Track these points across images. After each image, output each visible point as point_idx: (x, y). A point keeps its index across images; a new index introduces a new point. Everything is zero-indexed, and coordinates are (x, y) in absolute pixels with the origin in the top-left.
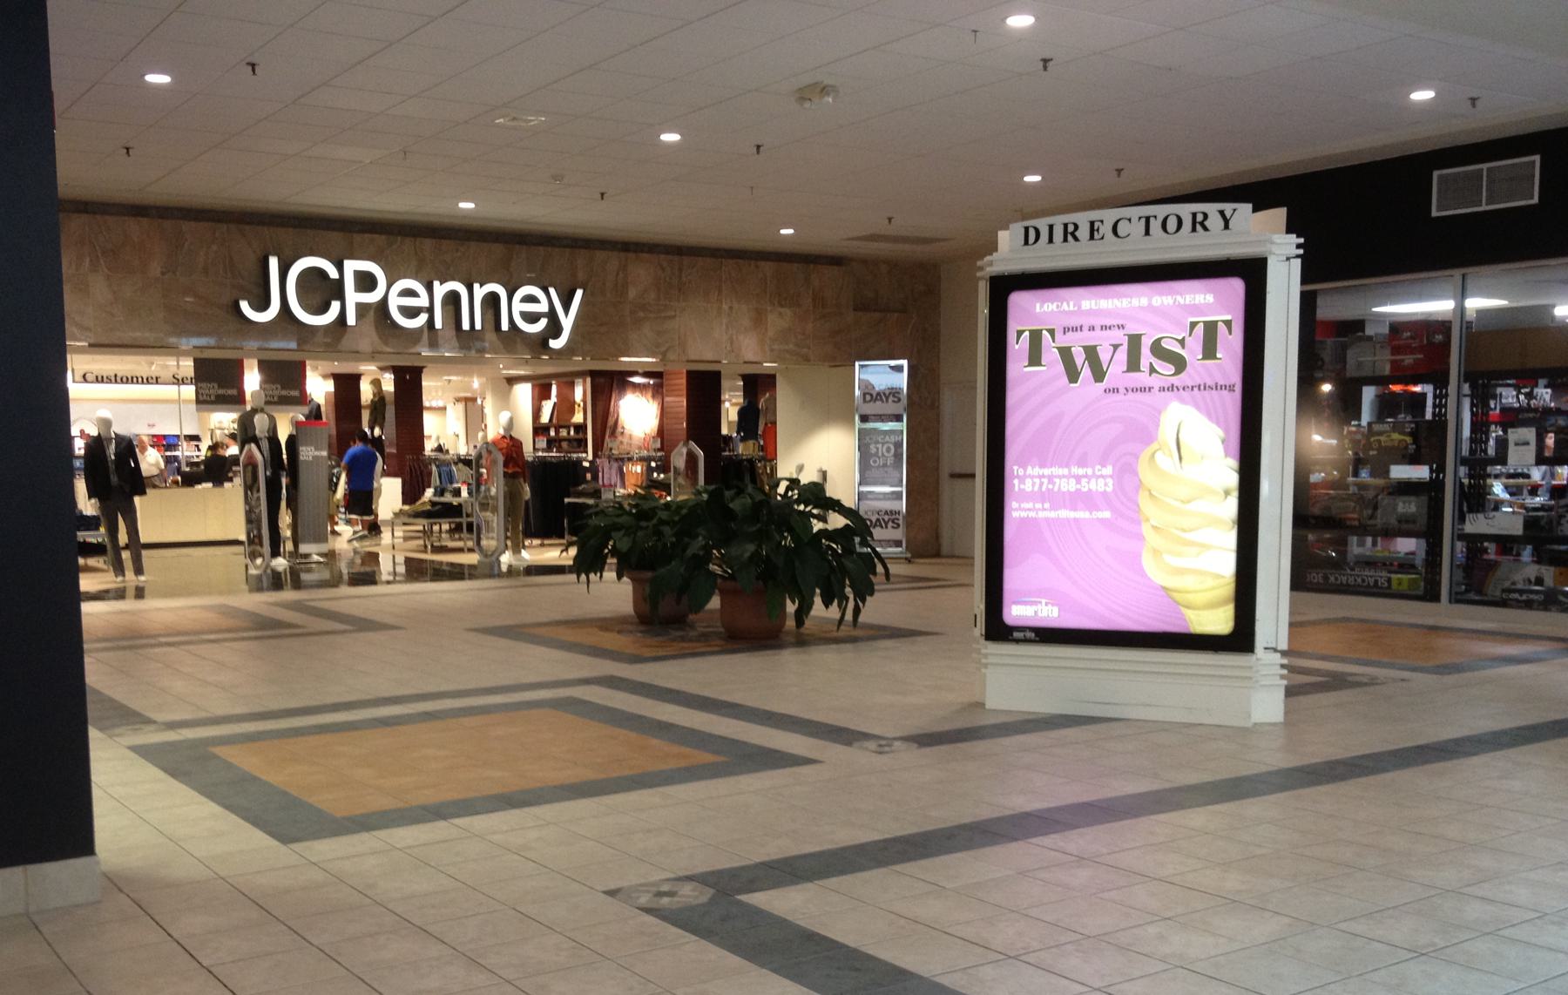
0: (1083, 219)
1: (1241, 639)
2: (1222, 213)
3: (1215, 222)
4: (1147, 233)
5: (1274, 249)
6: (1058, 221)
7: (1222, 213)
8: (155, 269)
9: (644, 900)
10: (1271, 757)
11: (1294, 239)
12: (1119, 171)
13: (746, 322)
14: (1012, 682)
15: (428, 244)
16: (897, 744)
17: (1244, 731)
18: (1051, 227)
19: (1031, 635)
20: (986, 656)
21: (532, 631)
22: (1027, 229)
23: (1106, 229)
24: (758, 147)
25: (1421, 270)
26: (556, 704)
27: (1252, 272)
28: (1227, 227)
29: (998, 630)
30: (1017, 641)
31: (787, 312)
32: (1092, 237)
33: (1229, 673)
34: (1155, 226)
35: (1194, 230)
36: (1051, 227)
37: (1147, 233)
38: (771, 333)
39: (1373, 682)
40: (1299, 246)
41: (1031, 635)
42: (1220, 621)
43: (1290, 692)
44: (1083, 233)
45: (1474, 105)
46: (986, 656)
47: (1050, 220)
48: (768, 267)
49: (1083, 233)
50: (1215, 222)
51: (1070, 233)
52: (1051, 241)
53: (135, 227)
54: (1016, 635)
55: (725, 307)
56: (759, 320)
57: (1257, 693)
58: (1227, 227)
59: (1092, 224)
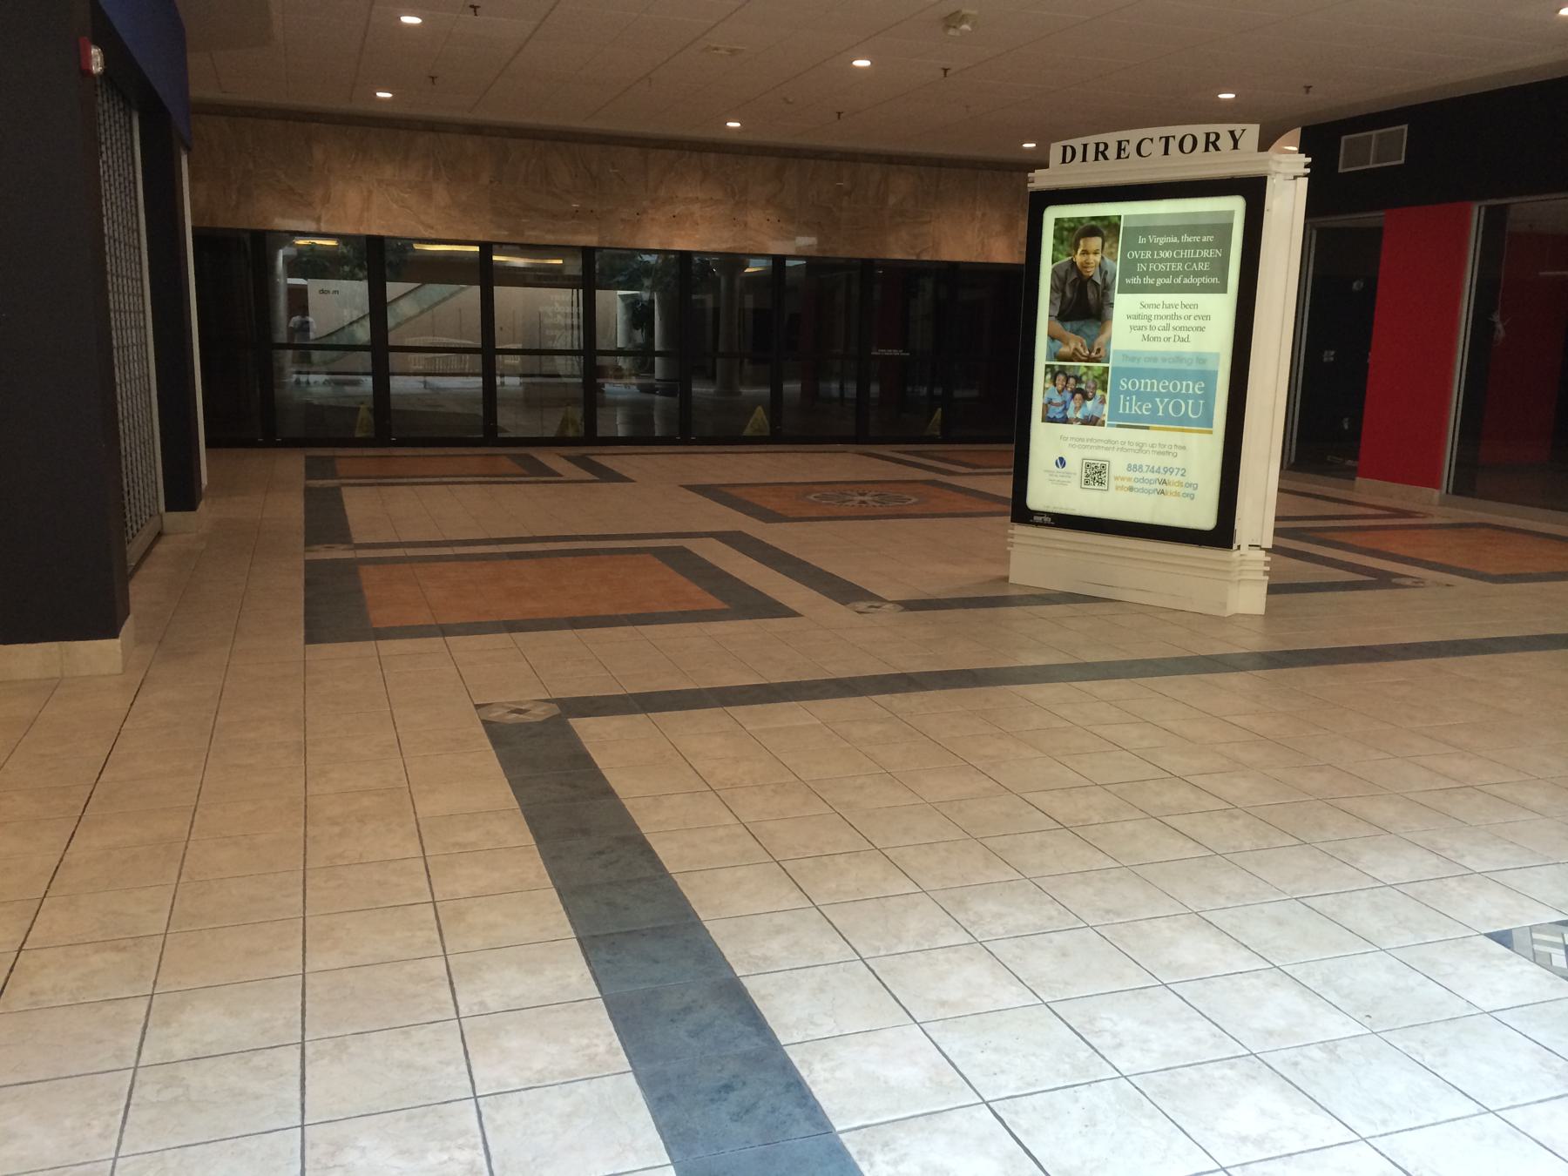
0: (1111, 138)
1: (1222, 535)
2: (1232, 133)
3: (1225, 142)
4: (1166, 153)
5: (1274, 167)
6: (1091, 140)
7: (1232, 133)
9: (495, 715)
10: (1252, 642)
12: (1308, 88)
14: (1033, 559)
15: (712, 157)
17: (1220, 621)
18: (1085, 146)
19: (1047, 519)
20: (1012, 536)
21: (734, 492)
22: (1065, 148)
23: (1131, 149)
24: (946, 70)
25: (1529, 194)
26: (659, 553)
27: (1253, 190)
28: (1235, 147)
29: (1022, 514)
30: (1037, 524)
32: (1119, 157)
33: (1176, 561)
34: (1173, 145)
35: (1207, 150)
36: (1085, 146)
37: (1166, 153)
41: (1047, 519)
42: (1205, 519)
43: (1272, 589)
44: (1112, 152)
46: (1012, 536)
47: (1084, 140)
49: (1112, 152)
50: (1225, 142)
51: (1101, 153)
52: (1084, 160)
54: (1037, 519)
55: (979, 213)
57: (1241, 586)
58: (1235, 147)
59: (1120, 143)
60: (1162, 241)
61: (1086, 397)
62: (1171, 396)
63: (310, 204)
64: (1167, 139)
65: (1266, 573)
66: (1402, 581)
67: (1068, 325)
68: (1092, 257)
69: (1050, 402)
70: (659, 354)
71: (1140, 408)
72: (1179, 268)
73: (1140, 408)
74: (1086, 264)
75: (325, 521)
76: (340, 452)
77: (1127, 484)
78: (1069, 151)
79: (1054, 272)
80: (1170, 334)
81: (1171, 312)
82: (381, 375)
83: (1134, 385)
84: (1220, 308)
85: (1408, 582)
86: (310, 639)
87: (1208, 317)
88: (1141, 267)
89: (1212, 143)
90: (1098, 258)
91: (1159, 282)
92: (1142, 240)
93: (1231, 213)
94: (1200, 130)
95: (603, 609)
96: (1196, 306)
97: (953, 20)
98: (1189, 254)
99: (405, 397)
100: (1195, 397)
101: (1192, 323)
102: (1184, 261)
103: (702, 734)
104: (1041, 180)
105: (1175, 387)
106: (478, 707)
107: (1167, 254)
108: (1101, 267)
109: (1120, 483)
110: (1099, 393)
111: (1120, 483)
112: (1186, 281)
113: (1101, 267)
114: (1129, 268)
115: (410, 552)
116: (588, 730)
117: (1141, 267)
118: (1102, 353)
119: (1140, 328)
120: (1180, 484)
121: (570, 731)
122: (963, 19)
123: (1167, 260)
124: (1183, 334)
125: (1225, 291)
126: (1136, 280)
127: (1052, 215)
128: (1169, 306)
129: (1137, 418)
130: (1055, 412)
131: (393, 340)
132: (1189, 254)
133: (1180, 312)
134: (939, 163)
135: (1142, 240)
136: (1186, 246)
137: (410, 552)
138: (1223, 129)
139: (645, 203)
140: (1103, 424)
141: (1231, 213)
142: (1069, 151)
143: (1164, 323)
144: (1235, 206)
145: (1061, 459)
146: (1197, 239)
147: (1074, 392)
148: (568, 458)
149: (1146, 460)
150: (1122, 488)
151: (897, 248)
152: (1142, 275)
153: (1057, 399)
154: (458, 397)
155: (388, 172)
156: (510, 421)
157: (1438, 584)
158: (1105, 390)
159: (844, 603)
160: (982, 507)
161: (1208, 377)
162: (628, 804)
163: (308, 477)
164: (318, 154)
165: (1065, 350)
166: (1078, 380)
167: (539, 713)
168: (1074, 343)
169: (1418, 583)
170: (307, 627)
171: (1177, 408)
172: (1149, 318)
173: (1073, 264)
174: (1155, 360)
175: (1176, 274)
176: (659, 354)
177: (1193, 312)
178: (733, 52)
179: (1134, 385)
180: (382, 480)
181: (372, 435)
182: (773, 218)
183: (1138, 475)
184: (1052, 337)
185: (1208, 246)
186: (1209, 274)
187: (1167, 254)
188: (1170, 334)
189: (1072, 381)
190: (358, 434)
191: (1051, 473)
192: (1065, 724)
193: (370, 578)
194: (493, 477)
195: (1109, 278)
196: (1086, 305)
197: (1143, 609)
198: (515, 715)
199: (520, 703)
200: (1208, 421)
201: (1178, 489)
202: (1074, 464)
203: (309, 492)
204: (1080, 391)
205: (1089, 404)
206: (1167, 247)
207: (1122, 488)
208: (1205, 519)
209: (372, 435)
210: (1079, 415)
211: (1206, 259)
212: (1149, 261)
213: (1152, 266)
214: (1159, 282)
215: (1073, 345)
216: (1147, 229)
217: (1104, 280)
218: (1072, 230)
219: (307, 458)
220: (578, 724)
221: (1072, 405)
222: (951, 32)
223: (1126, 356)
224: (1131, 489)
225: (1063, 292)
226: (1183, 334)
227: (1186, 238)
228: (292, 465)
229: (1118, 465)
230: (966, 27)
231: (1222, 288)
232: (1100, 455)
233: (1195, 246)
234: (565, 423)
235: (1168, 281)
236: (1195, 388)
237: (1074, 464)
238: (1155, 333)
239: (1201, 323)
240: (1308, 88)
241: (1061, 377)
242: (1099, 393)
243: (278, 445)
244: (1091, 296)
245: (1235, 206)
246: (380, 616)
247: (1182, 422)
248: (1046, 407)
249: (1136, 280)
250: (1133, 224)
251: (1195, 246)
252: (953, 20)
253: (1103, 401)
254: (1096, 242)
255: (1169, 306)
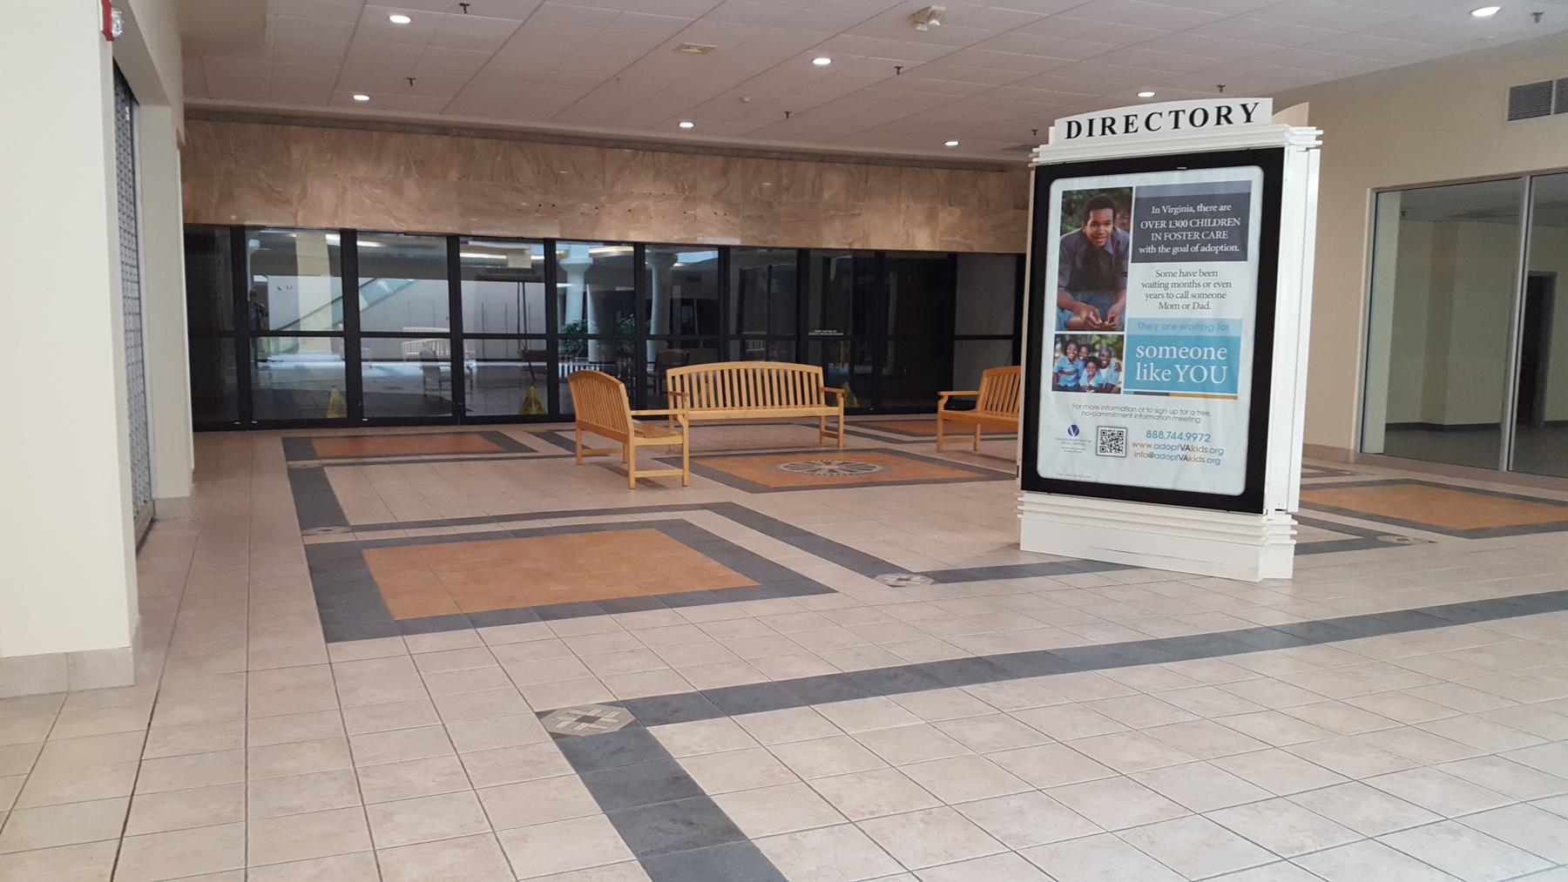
1: (1251, 500)
2: (1244, 106)
3: (1238, 115)
4: (1176, 126)
5: (1292, 140)
6: (1097, 116)
7: (1244, 106)
8: (453, 175)
9: (562, 725)
11: (1314, 132)
13: (920, 218)
14: (1046, 526)
16: (917, 578)
18: (1091, 121)
20: (1022, 503)
23: (1139, 123)
26: (663, 526)
27: (1271, 161)
28: (1248, 120)
31: (957, 211)
32: (1127, 131)
36: (1091, 121)
37: (1176, 126)
38: (941, 228)
39: (1403, 542)
40: (1318, 138)
42: (1234, 485)
43: (1301, 549)
44: (1119, 126)
45: (1537, 20)
46: (1022, 503)
47: (1090, 115)
48: (941, 174)
49: (1119, 126)
50: (1238, 115)
53: (439, 143)
56: (931, 217)
57: (1268, 546)
58: (1248, 120)
60: (1176, 211)
61: (1099, 365)
62: (1193, 362)
63: (288, 202)
64: (1177, 113)
65: (1292, 537)
66: (1387, 539)
67: (1079, 295)
68: (1103, 228)
69: (1061, 371)
70: (592, 337)
71: (1159, 375)
72: (1196, 236)
73: (1159, 375)
74: (1097, 235)
75: (317, 507)
76: (314, 433)
77: (1147, 451)
78: (1074, 126)
79: (1063, 243)
80: (1189, 301)
81: (1189, 279)
82: (353, 360)
83: (1151, 352)
84: (1242, 276)
85: (1394, 540)
86: (330, 637)
87: (1228, 285)
88: (1156, 237)
89: (1224, 116)
90: (1110, 229)
91: (1176, 250)
92: (1156, 211)
93: (1249, 183)
94: (1211, 105)
95: (631, 591)
96: (1215, 273)
97: (923, 15)
98: (1206, 222)
99: (375, 380)
100: (1219, 363)
101: (1212, 290)
102: (1200, 229)
103: (793, 733)
104: (1047, 154)
105: (1196, 354)
106: (540, 715)
107: (1183, 224)
108: (1113, 236)
109: (1138, 450)
110: (1114, 361)
111: (1138, 450)
112: (1204, 249)
113: (1113, 236)
114: (1143, 238)
115: (412, 533)
116: (675, 738)
117: (1156, 237)
118: (1116, 321)
119: (1157, 297)
120: (1205, 450)
121: (653, 746)
122: (933, 15)
123: (1183, 229)
124: (1203, 302)
125: (1245, 259)
126: (1151, 249)
127: (1058, 188)
128: (1187, 274)
129: (1155, 384)
130: (1067, 380)
131: (365, 326)
132: (1206, 222)
133: (1197, 279)
134: (868, 161)
135: (1156, 211)
136: (1201, 215)
137: (412, 533)
138: (1235, 103)
139: (603, 198)
140: (1119, 391)
141: (1249, 183)
142: (1074, 126)
143: (1182, 290)
144: (1253, 176)
145: (1074, 427)
146: (1214, 208)
147: (1086, 361)
148: (537, 435)
149: (1171, 426)
150: (1142, 454)
151: (833, 237)
152: (1157, 244)
153: (1069, 368)
154: (409, 380)
155: (362, 169)
156: (475, 403)
157: (1423, 542)
158: (1120, 358)
159: (872, 577)
160: (960, 473)
161: (1230, 344)
162: (763, 846)
163: (288, 459)
164: (296, 153)
165: (1076, 319)
166: (1091, 349)
167: (612, 721)
168: (1086, 313)
169: (1403, 542)
170: (324, 622)
171: (1199, 374)
172: (1166, 287)
173: (1082, 234)
174: (1174, 327)
175: (1193, 243)
176: (592, 337)
177: (1212, 280)
178: (704, 50)
179: (1151, 352)
180: (358, 459)
181: (345, 415)
182: (721, 213)
183: (1159, 441)
184: (1061, 307)
185: (1226, 215)
186: (1228, 242)
187: (1183, 224)
188: (1189, 301)
189: (1084, 349)
190: (330, 416)
191: (1063, 441)
192: (1189, 718)
193: (376, 562)
194: (460, 454)
195: (1121, 248)
196: (1098, 276)
197: (1175, 577)
198: (584, 725)
199: (588, 709)
200: (1231, 386)
201: (1203, 455)
202: (1088, 430)
203: (292, 473)
204: (1093, 359)
205: (1103, 372)
206: (1182, 216)
207: (1142, 454)
208: (1234, 485)
209: (345, 415)
210: (1092, 383)
211: (1224, 228)
212: (1163, 230)
213: (1168, 236)
214: (1176, 250)
215: (1084, 315)
216: (1158, 199)
217: (1117, 250)
218: (1081, 202)
219: (284, 439)
220: (660, 732)
221: (1085, 373)
222: (919, 27)
223: (1141, 324)
224: (1151, 455)
225: (1074, 264)
226: (1203, 302)
227: (1201, 208)
228: (270, 446)
229: (1136, 432)
230: (935, 22)
231: (1242, 255)
232: (1119, 422)
233: (1213, 215)
234: (527, 402)
235: (1185, 250)
236: (1216, 354)
237: (1088, 430)
238: (1174, 301)
239: (1221, 290)
240: (1537, 15)
241: (1072, 346)
242: (1114, 361)
243: (253, 428)
244: (1103, 265)
245: (1253, 176)
246: (401, 608)
247: (1205, 389)
248: (1056, 377)
249: (1151, 249)
250: (1144, 195)
251: (1213, 215)
252: (923, 15)
253: (1118, 369)
254: (1107, 214)
255: (1187, 274)
